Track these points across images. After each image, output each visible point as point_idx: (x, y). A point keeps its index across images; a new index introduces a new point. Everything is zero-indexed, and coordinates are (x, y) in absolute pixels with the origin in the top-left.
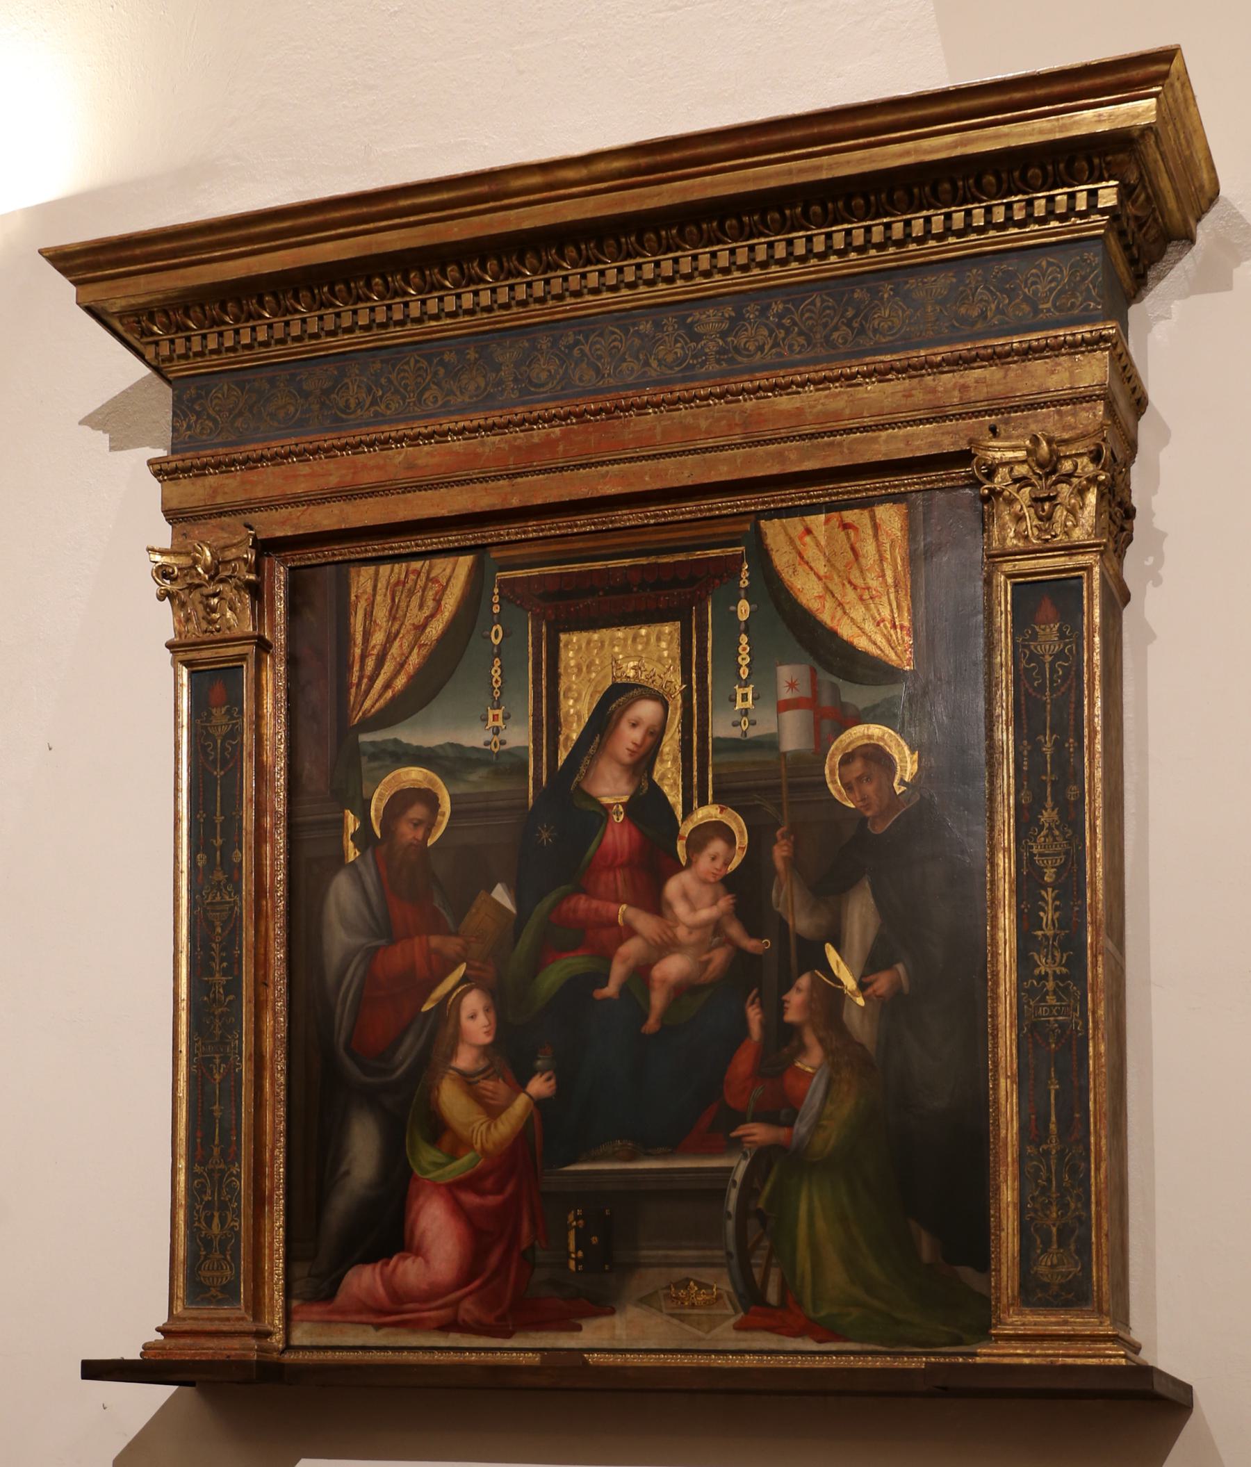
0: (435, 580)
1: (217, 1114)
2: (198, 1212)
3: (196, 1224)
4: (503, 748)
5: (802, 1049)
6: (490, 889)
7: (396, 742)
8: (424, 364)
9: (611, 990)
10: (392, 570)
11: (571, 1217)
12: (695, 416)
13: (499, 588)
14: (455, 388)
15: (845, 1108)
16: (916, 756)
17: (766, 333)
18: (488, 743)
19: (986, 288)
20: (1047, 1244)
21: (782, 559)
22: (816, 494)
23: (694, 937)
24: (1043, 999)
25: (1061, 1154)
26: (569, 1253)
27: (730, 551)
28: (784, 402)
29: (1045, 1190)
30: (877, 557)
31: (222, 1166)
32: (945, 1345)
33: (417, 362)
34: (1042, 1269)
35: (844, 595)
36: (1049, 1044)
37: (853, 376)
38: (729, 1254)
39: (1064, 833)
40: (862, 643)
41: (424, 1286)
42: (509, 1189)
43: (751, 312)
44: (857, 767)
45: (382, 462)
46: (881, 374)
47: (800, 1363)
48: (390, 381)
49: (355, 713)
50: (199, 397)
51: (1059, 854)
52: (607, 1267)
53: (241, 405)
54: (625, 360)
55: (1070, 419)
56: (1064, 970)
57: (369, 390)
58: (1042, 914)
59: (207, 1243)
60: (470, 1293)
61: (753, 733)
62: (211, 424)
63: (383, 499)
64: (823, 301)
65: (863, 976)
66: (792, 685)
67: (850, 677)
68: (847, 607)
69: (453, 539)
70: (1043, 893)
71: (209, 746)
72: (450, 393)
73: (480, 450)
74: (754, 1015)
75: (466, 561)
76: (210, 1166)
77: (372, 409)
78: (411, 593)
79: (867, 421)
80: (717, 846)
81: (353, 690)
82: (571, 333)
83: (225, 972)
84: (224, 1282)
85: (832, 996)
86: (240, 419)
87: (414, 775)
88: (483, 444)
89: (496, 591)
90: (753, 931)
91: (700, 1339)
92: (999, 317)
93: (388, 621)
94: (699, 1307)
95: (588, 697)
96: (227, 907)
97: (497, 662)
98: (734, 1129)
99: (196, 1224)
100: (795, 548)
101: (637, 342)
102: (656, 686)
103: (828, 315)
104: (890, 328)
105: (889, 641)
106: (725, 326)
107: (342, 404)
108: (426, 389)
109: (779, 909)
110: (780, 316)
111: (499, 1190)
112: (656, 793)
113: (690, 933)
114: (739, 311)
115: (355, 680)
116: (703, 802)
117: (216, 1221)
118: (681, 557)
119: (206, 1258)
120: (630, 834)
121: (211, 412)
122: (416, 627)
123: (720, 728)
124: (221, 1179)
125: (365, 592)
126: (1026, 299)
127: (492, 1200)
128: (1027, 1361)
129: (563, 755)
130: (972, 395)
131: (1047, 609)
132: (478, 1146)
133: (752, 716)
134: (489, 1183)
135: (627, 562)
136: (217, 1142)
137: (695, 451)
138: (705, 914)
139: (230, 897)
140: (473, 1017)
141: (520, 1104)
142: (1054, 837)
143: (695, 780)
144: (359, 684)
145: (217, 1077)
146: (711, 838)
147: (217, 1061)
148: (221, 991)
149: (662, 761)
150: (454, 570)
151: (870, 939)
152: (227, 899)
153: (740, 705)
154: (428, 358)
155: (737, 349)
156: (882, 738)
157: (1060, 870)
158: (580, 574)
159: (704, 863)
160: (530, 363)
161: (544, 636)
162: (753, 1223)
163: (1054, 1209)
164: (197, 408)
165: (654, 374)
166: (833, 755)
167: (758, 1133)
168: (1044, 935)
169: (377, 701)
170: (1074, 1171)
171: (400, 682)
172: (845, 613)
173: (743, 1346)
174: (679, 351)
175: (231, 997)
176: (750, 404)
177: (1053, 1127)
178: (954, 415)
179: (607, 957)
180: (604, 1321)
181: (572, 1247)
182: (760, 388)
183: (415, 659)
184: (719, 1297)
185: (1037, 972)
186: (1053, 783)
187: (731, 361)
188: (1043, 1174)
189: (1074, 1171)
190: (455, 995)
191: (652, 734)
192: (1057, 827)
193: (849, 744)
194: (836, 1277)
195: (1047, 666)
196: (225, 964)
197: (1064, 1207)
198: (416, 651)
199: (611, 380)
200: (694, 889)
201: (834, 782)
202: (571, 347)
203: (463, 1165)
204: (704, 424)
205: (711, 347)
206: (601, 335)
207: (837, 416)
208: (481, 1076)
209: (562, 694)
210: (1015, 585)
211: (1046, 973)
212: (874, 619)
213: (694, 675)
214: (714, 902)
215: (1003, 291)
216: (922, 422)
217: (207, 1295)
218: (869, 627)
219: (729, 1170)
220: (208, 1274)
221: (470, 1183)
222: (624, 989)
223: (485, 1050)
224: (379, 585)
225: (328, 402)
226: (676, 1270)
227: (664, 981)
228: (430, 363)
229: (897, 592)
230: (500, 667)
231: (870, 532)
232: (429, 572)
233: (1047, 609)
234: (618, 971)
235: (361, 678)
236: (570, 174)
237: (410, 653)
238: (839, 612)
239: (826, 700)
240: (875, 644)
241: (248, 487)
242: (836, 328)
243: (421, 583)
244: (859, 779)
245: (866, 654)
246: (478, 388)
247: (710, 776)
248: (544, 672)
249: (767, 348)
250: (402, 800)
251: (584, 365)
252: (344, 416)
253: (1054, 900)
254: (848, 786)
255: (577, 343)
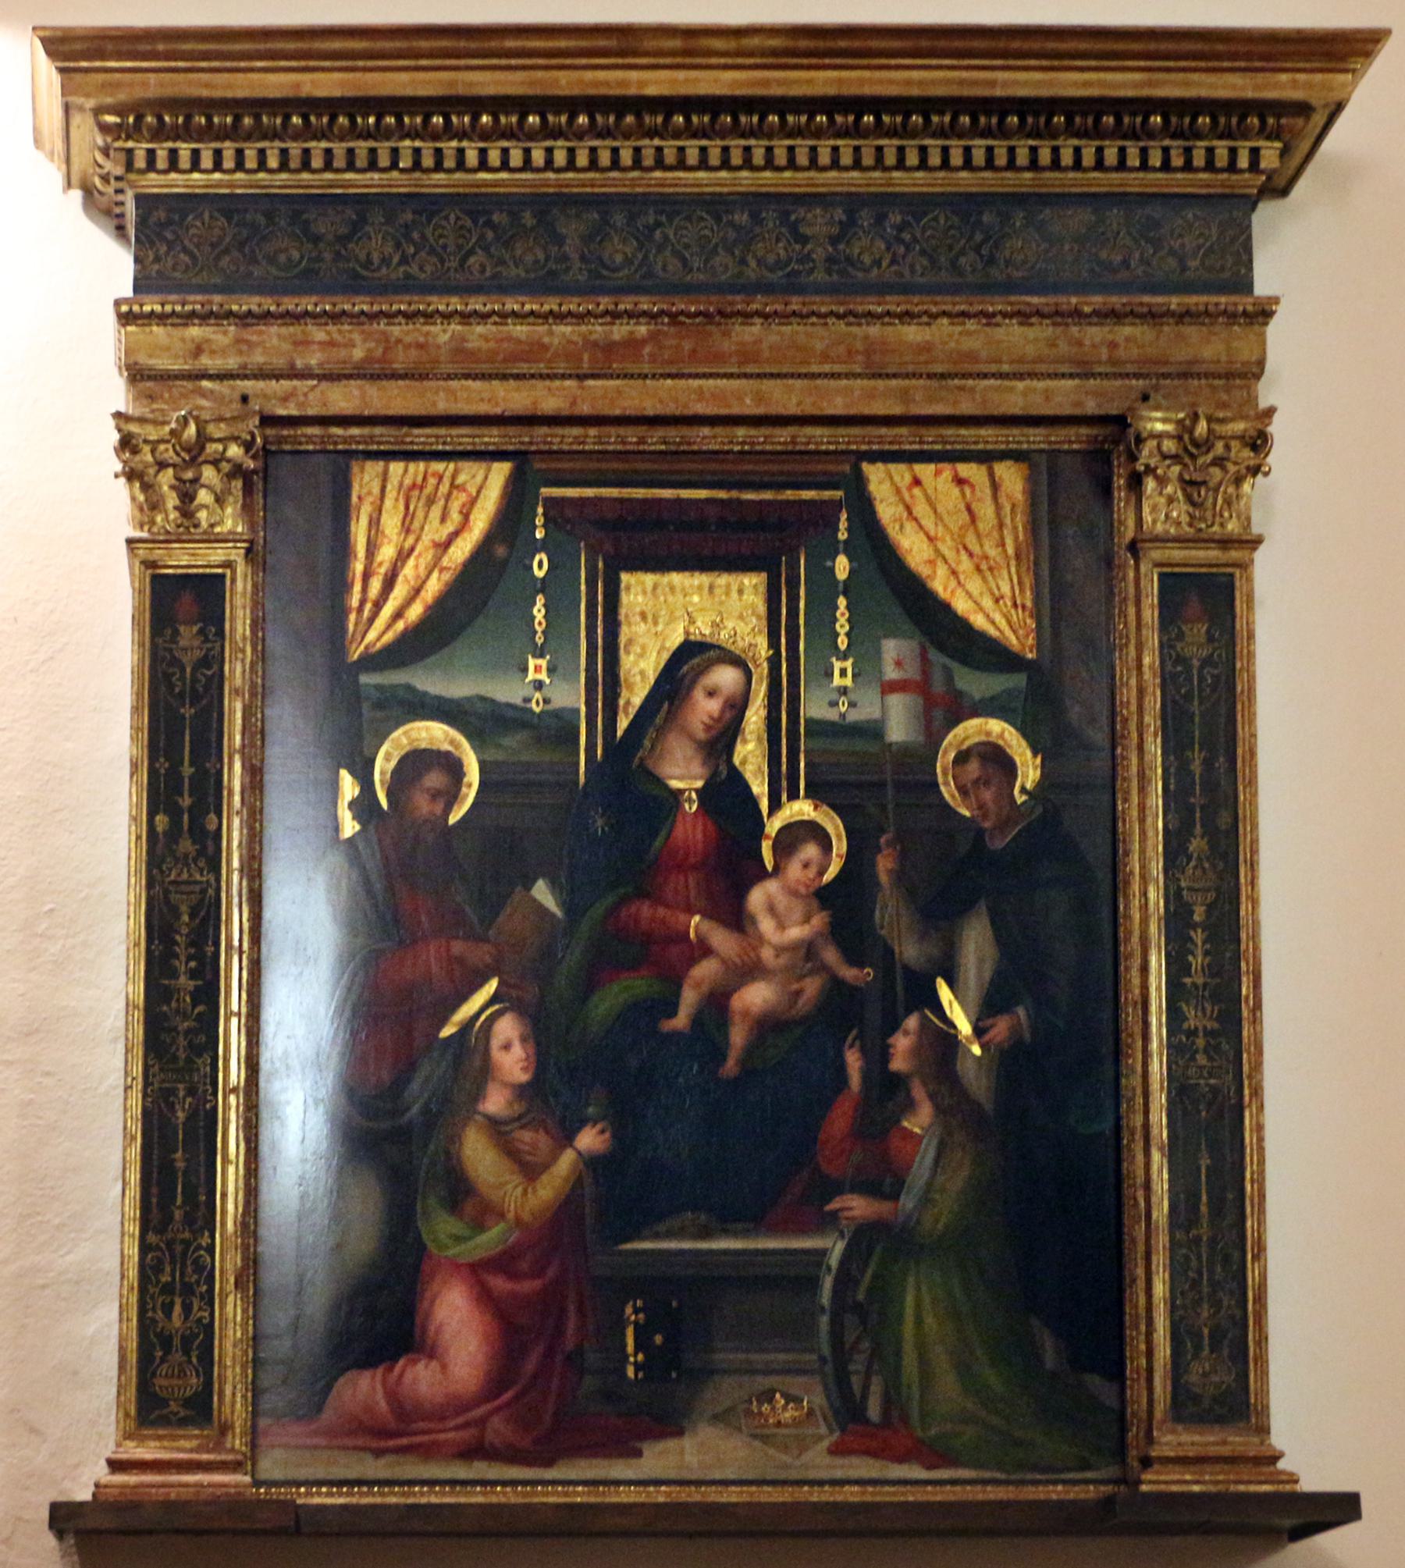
0: (461, 488)
1: (180, 1165)
2: (152, 1297)
3: (150, 1314)
4: (549, 707)
5: (910, 1106)
6: (528, 885)
7: (409, 688)
8: (469, 223)
9: (681, 1021)
10: (406, 471)
11: (629, 1310)
12: (808, 335)
13: (544, 507)
14: (507, 257)
15: (957, 1180)
16: (1038, 760)
17: (883, 247)
18: (528, 700)
19: (1130, 234)
20: (1198, 1348)
21: (887, 511)
22: (932, 442)
23: (783, 960)
24: (1193, 1058)
25: (1213, 1241)
26: (627, 1357)
27: (827, 494)
28: (912, 333)
29: (1195, 1284)
30: (995, 522)
31: (187, 1235)
32: (1069, 1470)
33: (458, 218)
34: (1193, 1378)
35: (959, 562)
36: (1199, 1112)
37: (994, 315)
38: (823, 1360)
39: (1214, 866)
40: (979, 621)
41: (439, 1399)
42: (551, 1272)
43: (865, 218)
44: (973, 768)
45: (422, 339)
46: (1024, 317)
47: (912, 1496)
48: (423, 237)
49: (354, 646)
50: (169, 223)
51: (1208, 890)
52: (674, 1375)
53: (228, 240)
54: (717, 254)
55: (1225, 397)
56: (1216, 1025)
57: (398, 245)
58: (1190, 958)
59: (166, 1342)
60: (499, 1409)
61: (853, 716)
62: (187, 259)
63: (417, 384)
64: (947, 218)
65: (978, 1020)
66: (898, 664)
67: (965, 660)
68: (962, 577)
69: (491, 438)
70: (1192, 933)
71: (174, 674)
72: (502, 262)
73: (546, 340)
74: (853, 1060)
75: (500, 472)
76: (170, 1236)
77: (402, 269)
78: (431, 501)
79: (1006, 368)
80: (811, 851)
81: (352, 617)
82: (651, 211)
83: (193, 974)
84: (188, 1393)
85: (945, 1040)
86: (227, 259)
87: (433, 733)
88: (551, 333)
89: (540, 510)
90: (854, 958)
91: (786, 1466)
92: (1142, 268)
93: (399, 534)
94: (786, 1426)
95: (654, 654)
96: (197, 888)
97: (540, 600)
98: (828, 1202)
99: (150, 1314)
100: (902, 500)
101: (732, 235)
102: (738, 647)
103: (953, 236)
104: (1024, 262)
105: (1009, 622)
106: (835, 230)
107: (362, 256)
108: (471, 252)
109: (883, 932)
110: (900, 228)
111: (538, 1273)
112: (737, 779)
113: (777, 956)
114: (851, 213)
115: (355, 602)
116: (793, 796)
117: (178, 1309)
118: (767, 495)
119: (163, 1360)
120: (705, 826)
121: (186, 242)
122: (436, 545)
123: (814, 707)
124: (184, 1254)
125: (369, 493)
126: (1172, 252)
127: (528, 1286)
128: (1196, 1488)
129: (623, 723)
130: (1121, 353)
131: (1194, 606)
132: (511, 1216)
133: (853, 696)
134: (524, 1265)
135: (702, 494)
136: (179, 1201)
137: (806, 376)
138: (795, 933)
139: (202, 875)
140: (507, 1047)
141: (566, 1161)
142: (1204, 869)
143: (784, 767)
144: (360, 609)
145: (181, 1115)
146: (804, 841)
147: (181, 1094)
148: (188, 999)
149: (745, 741)
150: (486, 478)
151: (987, 975)
152: (198, 877)
153: (837, 681)
154: (473, 215)
155: (848, 259)
156: (1001, 736)
157: (1210, 908)
158: (645, 501)
159: (794, 870)
160: (601, 241)
161: (600, 573)
162: (850, 1320)
163: (1206, 1306)
164: (169, 236)
165: (753, 275)
166: (945, 752)
167: (857, 1206)
168: (1194, 984)
169: (384, 633)
170: (1226, 1260)
171: (415, 612)
172: (959, 583)
173: (839, 1474)
174: (782, 252)
175: (200, 1008)
176: (874, 330)
177: (1204, 1209)
178: (1100, 374)
179: (675, 981)
180: (671, 1444)
181: (630, 1348)
182: (888, 313)
183: (434, 586)
184: (811, 1413)
185: (1185, 1026)
186: (1202, 807)
187: (842, 273)
188: (1194, 1263)
189: (1226, 1260)
190: (483, 1017)
191: (732, 706)
192: (1208, 859)
193: (965, 739)
194: (948, 1384)
195: (1195, 672)
196: (193, 964)
197: (1217, 1304)
198: (435, 575)
199: (701, 277)
200: (782, 901)
201: (946, 784)
202: (651, 229)
203: (490, 1239)
204: (819, 346)
205: (819, 254)
206: (689, 218)
207: (971, 356)
208: (516, 1124)
209: (622, 646)
210: (1161, 576)
211: (1196, 1028)
212: (992, 594)
213: (783, 640)
214: (807, 920)
215: (1148, 241)
216: (1063, 376)
217: (165, 1411)
218: (987, 603)
219: (823, 1253)
220: (164, 1382)
221: (503, 1262)
222: (697, 1020)
223: (521, 1091)
224: (389, 487)
225: (343, 252)
226: (759, 1379)
227: (746, 1013)
228: (475, 222)
229: (1018, 566)
230: (545, 605)
231: (988, 491)
232: (454, 477)
233: (1194, 606)
234: (689, 999)
235: (363, 602)
236: (718, 44)
237: (428, 576)
238: (953, 583)
239: (938, 686)
240: (993, 622)
241: (244, 348)
242: (962, 253)
243: (444, 488)
244: (976, 782)
245: (982, 636)
246: (537, 261)
247: (802, 765)
248: (600, 618)
249: (884, 264)
250: (416, 762)
251: (668, 253)
252: (365, 273)
253: (1204, 943)
254: (963, 790)
255: (658, 224)
